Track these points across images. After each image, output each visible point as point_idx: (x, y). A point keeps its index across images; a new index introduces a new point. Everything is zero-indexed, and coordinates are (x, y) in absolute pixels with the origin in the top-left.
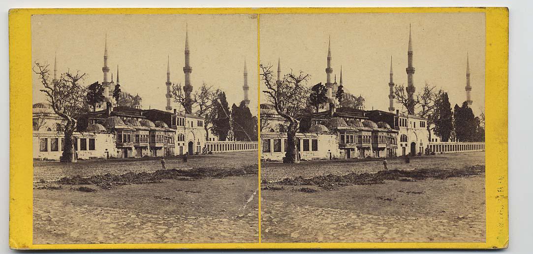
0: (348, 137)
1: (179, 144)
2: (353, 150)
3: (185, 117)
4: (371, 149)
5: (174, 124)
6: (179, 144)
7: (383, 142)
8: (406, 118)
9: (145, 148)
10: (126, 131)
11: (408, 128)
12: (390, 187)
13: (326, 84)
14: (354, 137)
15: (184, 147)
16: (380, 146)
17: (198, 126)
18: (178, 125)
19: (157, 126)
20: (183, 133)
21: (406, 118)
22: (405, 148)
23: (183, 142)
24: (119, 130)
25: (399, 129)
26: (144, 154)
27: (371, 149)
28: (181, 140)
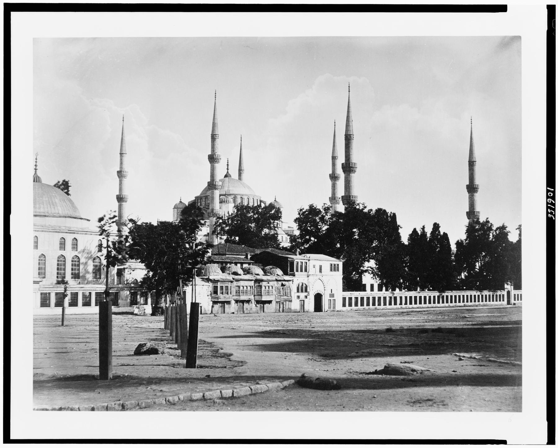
0: (222, 288)
1: (298, 297)
2: (229, 303)
3: (309, 260)
4: (253, 302)
5: (292, 270)
6: (298, 297)
7: (268, 293)
8: (307, 261)
9: (248, 301)
10: (224, 281)
11: (310, 273)
12: (506, 366)
13: (129, 233)
14: (229, 288)
15: (306, 300)
16: (264, 298)
17: (331, 270)
18: (297, 271)
19: (265, 273)
20: (305, 282)
21: (307, 261)
22: (304, 301)
23: (306, 294)
24: (215, 281)
25: (294, 275)
26: (247, 309)
27: (253, 302)
28: (302, 291)
